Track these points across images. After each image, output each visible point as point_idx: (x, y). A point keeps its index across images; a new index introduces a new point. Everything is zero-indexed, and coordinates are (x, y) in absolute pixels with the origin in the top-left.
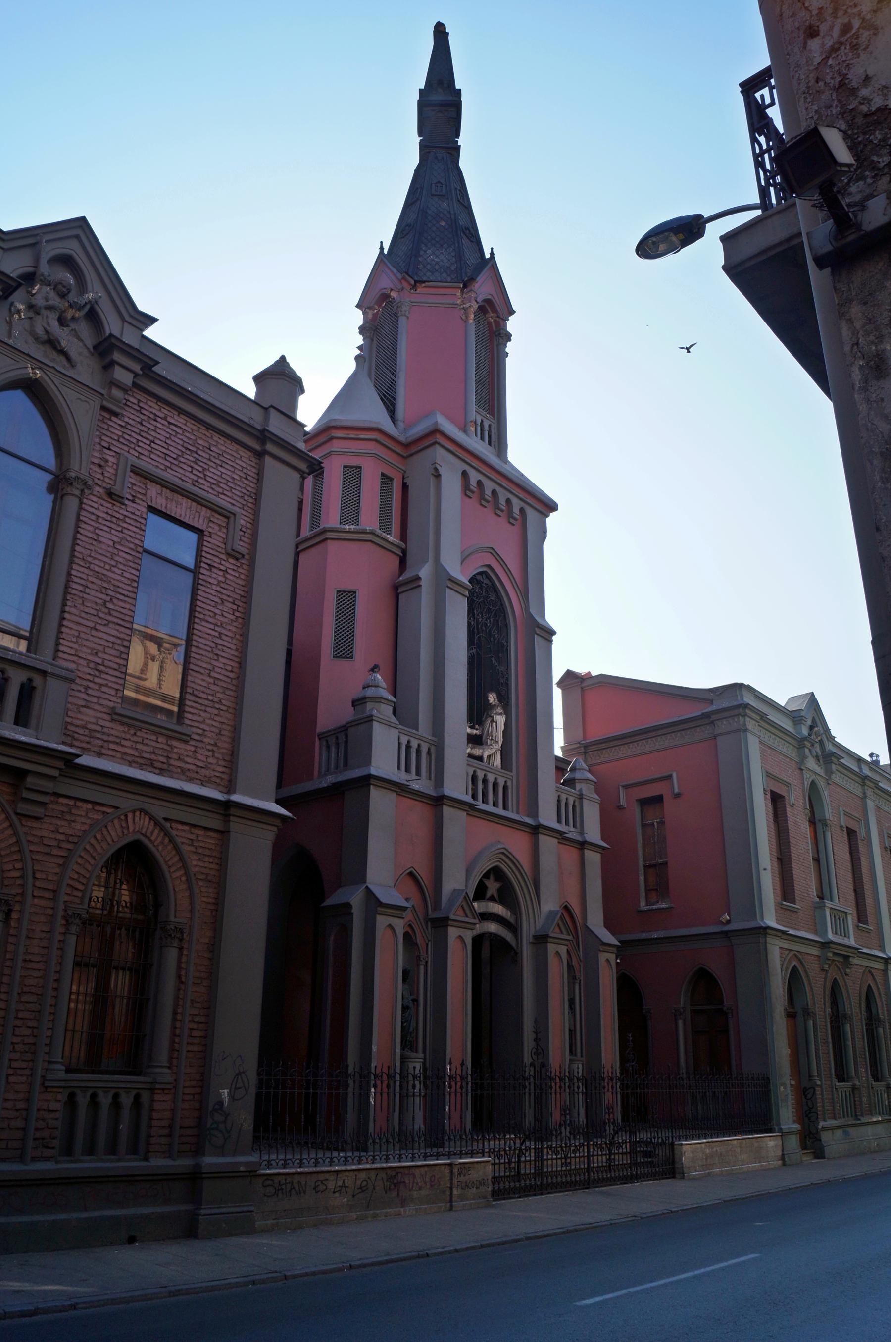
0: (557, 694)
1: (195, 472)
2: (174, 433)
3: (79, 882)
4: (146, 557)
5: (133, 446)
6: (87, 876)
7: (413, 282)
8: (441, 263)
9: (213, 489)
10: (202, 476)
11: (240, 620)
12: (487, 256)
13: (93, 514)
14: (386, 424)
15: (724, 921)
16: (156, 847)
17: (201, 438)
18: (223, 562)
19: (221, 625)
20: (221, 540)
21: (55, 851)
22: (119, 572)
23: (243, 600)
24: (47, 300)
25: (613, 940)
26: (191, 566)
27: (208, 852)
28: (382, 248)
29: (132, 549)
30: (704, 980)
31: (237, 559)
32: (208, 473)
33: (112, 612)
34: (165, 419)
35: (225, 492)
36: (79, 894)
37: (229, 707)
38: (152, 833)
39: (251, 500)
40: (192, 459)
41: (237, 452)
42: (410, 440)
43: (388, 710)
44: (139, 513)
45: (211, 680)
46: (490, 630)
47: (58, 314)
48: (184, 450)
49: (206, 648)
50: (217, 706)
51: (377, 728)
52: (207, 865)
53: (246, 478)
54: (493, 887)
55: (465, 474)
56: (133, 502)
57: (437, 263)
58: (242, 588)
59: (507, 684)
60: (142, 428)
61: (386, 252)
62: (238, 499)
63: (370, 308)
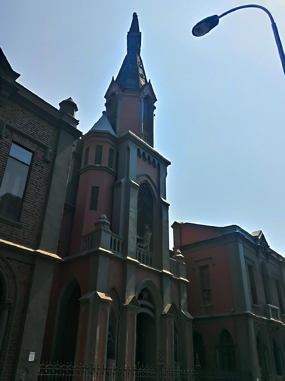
0: (171, 231)
4: (9, 159)
7: (123, 89)
9: (40, 138)
10: (36, 133)
12: (148, 82)
14: (112, 132)
25: (192, 317)
26: (29, 163)
28: (113, 79)
29: (4, 155)
30: (225, 334)
32: (38, 132)
34: (22, 111)
43: (108, 228)
44: (8, 142)
45: (33, 206)
48: (29, 123)
49: (32, 194)
50: (35, 216)
51: (103, 234)
53: (53, 136)
54: (145, 295)
56: (6, 138)
57: (132, 83)
60: (12, 113)
61: (115, 80)
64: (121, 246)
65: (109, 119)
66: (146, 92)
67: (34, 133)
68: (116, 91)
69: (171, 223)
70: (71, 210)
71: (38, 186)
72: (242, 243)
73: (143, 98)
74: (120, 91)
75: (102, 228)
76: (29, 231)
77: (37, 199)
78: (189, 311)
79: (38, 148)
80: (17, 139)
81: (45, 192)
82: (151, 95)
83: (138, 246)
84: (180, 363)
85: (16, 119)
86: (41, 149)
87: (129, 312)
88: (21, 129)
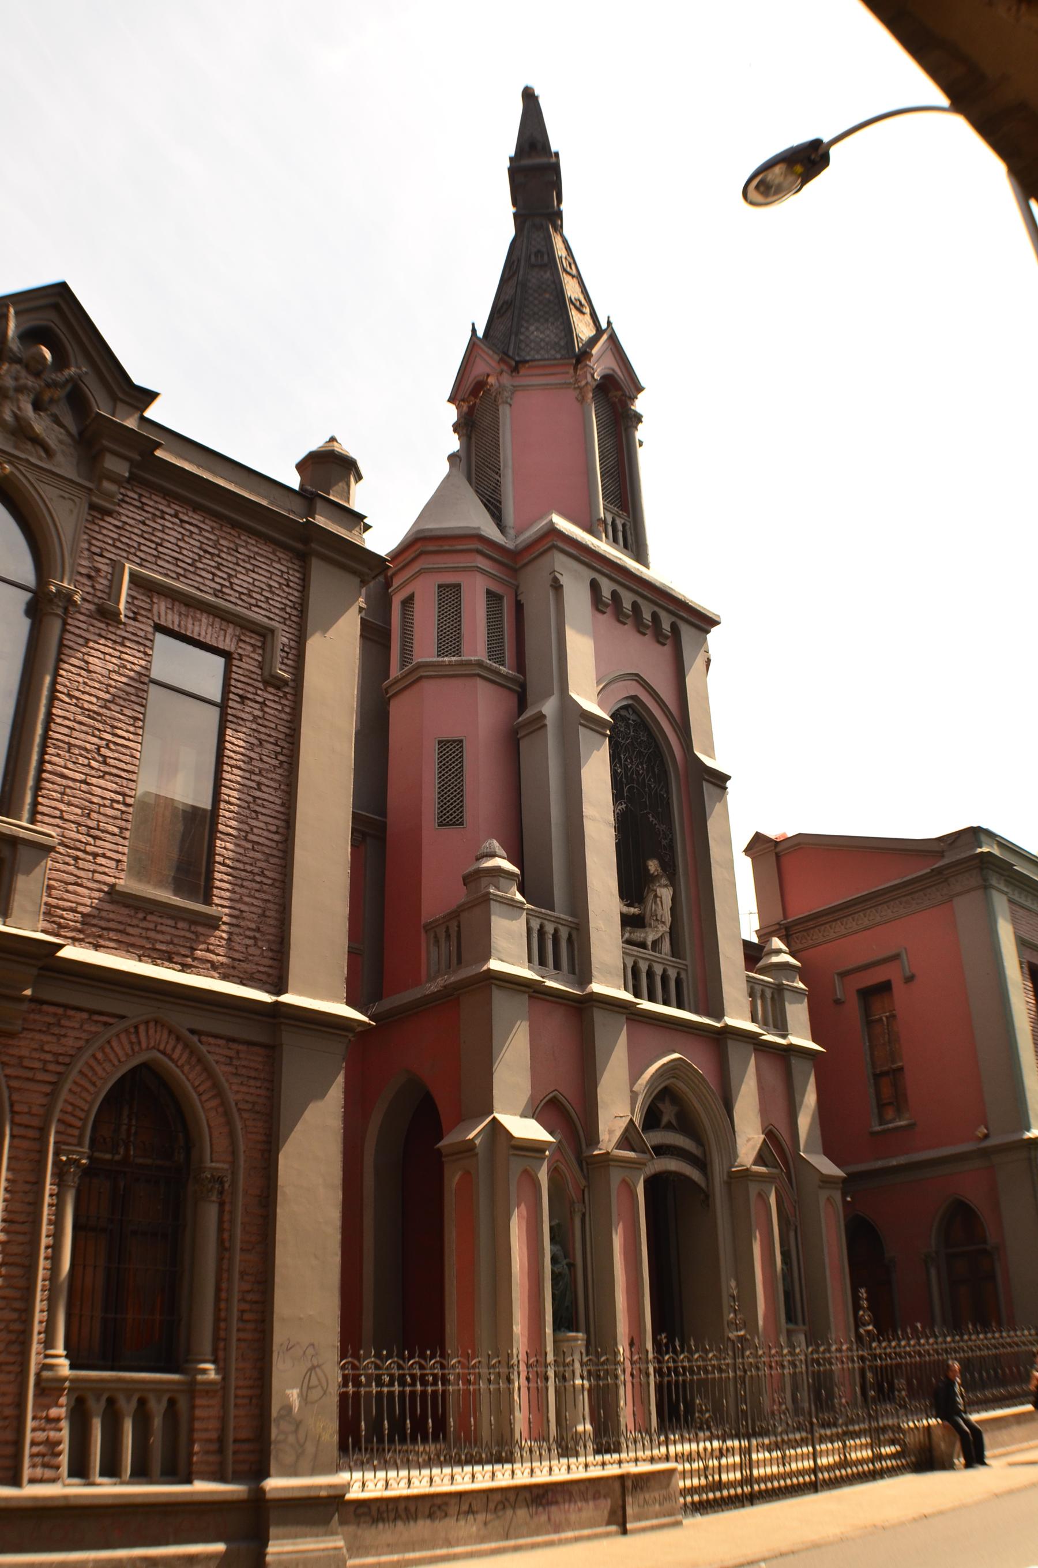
1: (217, 579)
2: (188, 533)
3: (74, 1116)
4: (153, 689)
5: (133, 550)
6: (86, 1108)
7: (513, 363)
8: (547, 339)
9: (243, 600)
10: (227, 584)
11: (285, 766)
13: (81, 637)
14: (491, 531)
15: (980, 1135)
16: (181, 1067)
17: (225, 538)
18: (259, 692)
19: (260, 774)
20: (256, 663)
21: (41, 1076)
22: (118, 708)
23: (289, 739)
24: (16, 379)
26: (217, 698)
27: (253, 1074)
28: (474, 331)
30: (962, 1218)
31: (278, 688)
32: (236, 581)
33: (109, 760)
34: (176, 516)
35: (260, 604)
36: (76, 1132)
37: (274, 879)
38: (173, 1050)
39: (295, 612)
40: (213, 564)
41: (274, 553)
42: (520, 547)
44: (142, 634)
45: (249, 845)
46: (644, 779)
47: (32, 396)
48: (202, 553)
50: (258, 879)
52: (252, 1090)
53: (288, 586)
54: (668, 1114)
55: (594, 586)
56: (135, 619)
57: (542, 340)
58: (288, 725)
59: (671, 847)
62: (277, 611)
63: (463, 400)
64: (563, 944)
65: (474, 480)
66: (599, 366)
67: (222, 585)
68: (488, 375)
69: (740, 840)
70: (376, 836)
71: (257, 771)
72: (1006, 893)
73: (589, 388)
74: (502, 372)
75: (489, 893)
76: (248, 933)
77: (257, 819)
78: (829, 1152)
79: (243, 638)
80: (170, 617)
81: (283, 791)
82: (620, 373)
83: (628, 942)
84: (804, 1323)
85: (160, 549)
86: (252, 641)
87: (616, 1177)
88: (178, 579)
